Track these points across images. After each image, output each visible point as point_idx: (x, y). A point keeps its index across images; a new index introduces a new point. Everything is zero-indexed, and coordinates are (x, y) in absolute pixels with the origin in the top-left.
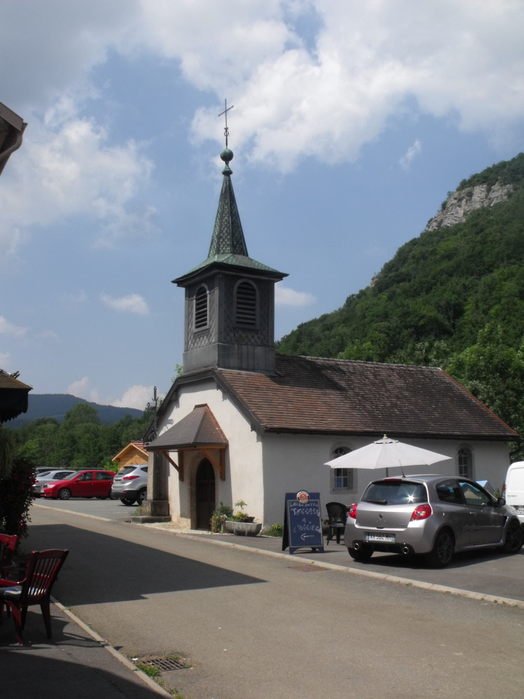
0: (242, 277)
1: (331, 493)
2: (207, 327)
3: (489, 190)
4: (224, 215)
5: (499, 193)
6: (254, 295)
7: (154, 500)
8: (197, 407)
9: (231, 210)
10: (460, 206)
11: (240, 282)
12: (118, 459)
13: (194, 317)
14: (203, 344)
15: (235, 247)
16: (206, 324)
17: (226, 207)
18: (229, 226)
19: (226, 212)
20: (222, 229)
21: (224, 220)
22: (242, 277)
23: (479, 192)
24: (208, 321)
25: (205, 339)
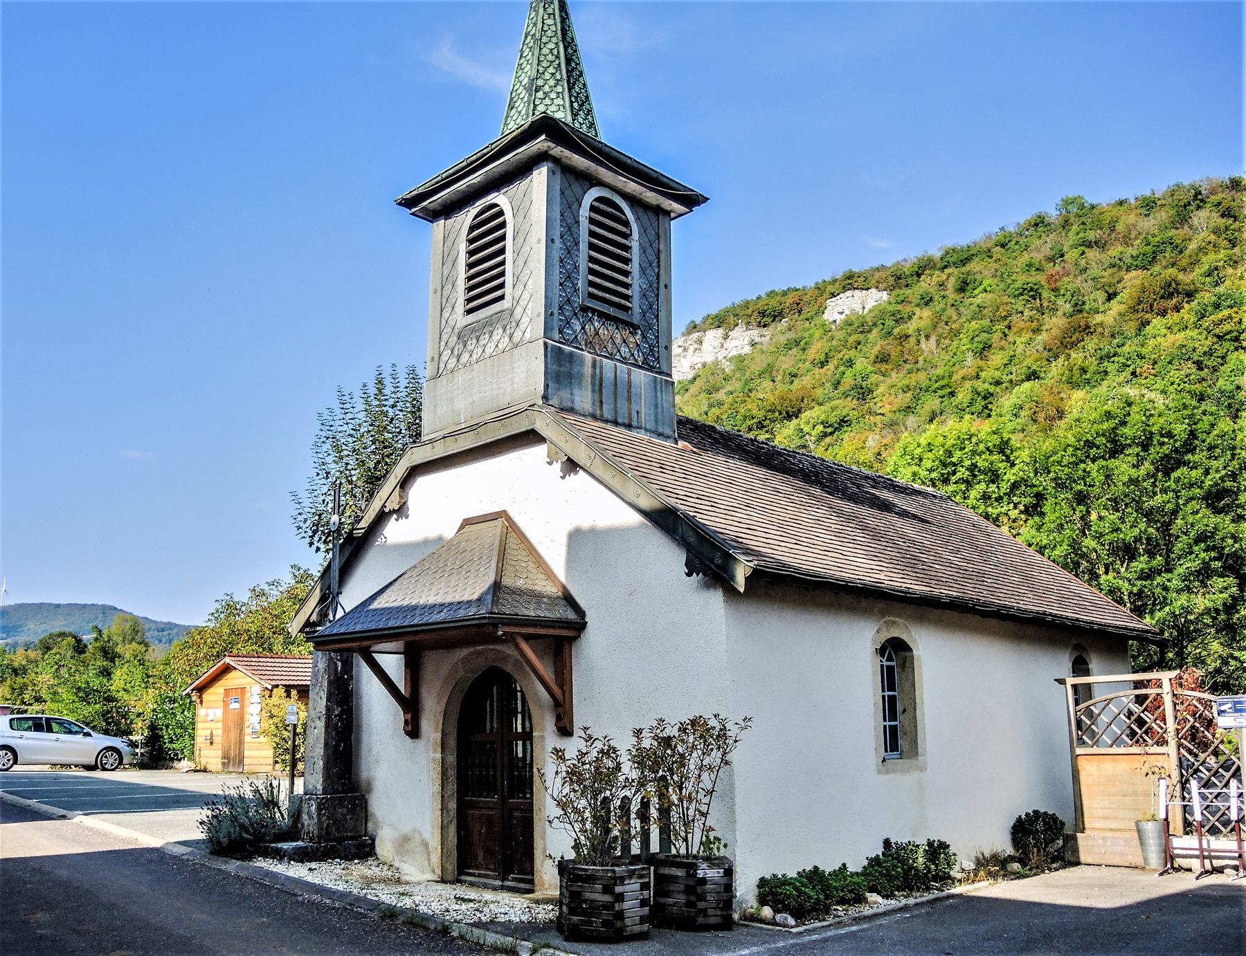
0: (600, 183)
1: (879, 772)
2: (505, 304)
3: (726, 337)
4: (544, 39)
5: (741, 340)
6: (626, 236)
7: (325, 792)
8: (467, 522)
9: (564, 32)
10: (685, 357)
11: (594, 193)
12: (492, 809)
13: (461, 284)
14: (489, 351)
15: (576, 115)
16: (502, 298)
17: (550, 22)
18: (559, 65)
19: (549, 33)
20: (541, 70)
21: (545, 51)
22: (600, 183)
23: (713, 337)
24: (508, 290)
25: (496, 338)
